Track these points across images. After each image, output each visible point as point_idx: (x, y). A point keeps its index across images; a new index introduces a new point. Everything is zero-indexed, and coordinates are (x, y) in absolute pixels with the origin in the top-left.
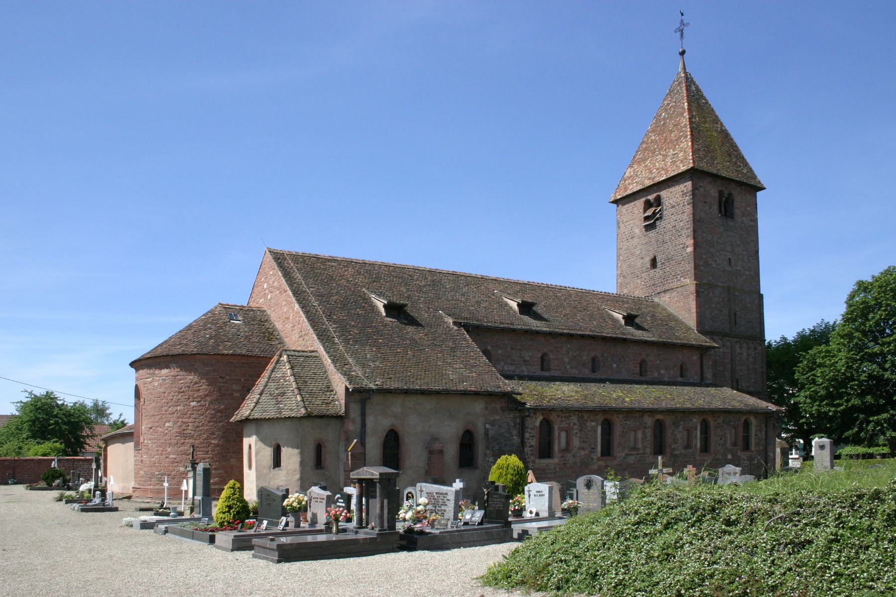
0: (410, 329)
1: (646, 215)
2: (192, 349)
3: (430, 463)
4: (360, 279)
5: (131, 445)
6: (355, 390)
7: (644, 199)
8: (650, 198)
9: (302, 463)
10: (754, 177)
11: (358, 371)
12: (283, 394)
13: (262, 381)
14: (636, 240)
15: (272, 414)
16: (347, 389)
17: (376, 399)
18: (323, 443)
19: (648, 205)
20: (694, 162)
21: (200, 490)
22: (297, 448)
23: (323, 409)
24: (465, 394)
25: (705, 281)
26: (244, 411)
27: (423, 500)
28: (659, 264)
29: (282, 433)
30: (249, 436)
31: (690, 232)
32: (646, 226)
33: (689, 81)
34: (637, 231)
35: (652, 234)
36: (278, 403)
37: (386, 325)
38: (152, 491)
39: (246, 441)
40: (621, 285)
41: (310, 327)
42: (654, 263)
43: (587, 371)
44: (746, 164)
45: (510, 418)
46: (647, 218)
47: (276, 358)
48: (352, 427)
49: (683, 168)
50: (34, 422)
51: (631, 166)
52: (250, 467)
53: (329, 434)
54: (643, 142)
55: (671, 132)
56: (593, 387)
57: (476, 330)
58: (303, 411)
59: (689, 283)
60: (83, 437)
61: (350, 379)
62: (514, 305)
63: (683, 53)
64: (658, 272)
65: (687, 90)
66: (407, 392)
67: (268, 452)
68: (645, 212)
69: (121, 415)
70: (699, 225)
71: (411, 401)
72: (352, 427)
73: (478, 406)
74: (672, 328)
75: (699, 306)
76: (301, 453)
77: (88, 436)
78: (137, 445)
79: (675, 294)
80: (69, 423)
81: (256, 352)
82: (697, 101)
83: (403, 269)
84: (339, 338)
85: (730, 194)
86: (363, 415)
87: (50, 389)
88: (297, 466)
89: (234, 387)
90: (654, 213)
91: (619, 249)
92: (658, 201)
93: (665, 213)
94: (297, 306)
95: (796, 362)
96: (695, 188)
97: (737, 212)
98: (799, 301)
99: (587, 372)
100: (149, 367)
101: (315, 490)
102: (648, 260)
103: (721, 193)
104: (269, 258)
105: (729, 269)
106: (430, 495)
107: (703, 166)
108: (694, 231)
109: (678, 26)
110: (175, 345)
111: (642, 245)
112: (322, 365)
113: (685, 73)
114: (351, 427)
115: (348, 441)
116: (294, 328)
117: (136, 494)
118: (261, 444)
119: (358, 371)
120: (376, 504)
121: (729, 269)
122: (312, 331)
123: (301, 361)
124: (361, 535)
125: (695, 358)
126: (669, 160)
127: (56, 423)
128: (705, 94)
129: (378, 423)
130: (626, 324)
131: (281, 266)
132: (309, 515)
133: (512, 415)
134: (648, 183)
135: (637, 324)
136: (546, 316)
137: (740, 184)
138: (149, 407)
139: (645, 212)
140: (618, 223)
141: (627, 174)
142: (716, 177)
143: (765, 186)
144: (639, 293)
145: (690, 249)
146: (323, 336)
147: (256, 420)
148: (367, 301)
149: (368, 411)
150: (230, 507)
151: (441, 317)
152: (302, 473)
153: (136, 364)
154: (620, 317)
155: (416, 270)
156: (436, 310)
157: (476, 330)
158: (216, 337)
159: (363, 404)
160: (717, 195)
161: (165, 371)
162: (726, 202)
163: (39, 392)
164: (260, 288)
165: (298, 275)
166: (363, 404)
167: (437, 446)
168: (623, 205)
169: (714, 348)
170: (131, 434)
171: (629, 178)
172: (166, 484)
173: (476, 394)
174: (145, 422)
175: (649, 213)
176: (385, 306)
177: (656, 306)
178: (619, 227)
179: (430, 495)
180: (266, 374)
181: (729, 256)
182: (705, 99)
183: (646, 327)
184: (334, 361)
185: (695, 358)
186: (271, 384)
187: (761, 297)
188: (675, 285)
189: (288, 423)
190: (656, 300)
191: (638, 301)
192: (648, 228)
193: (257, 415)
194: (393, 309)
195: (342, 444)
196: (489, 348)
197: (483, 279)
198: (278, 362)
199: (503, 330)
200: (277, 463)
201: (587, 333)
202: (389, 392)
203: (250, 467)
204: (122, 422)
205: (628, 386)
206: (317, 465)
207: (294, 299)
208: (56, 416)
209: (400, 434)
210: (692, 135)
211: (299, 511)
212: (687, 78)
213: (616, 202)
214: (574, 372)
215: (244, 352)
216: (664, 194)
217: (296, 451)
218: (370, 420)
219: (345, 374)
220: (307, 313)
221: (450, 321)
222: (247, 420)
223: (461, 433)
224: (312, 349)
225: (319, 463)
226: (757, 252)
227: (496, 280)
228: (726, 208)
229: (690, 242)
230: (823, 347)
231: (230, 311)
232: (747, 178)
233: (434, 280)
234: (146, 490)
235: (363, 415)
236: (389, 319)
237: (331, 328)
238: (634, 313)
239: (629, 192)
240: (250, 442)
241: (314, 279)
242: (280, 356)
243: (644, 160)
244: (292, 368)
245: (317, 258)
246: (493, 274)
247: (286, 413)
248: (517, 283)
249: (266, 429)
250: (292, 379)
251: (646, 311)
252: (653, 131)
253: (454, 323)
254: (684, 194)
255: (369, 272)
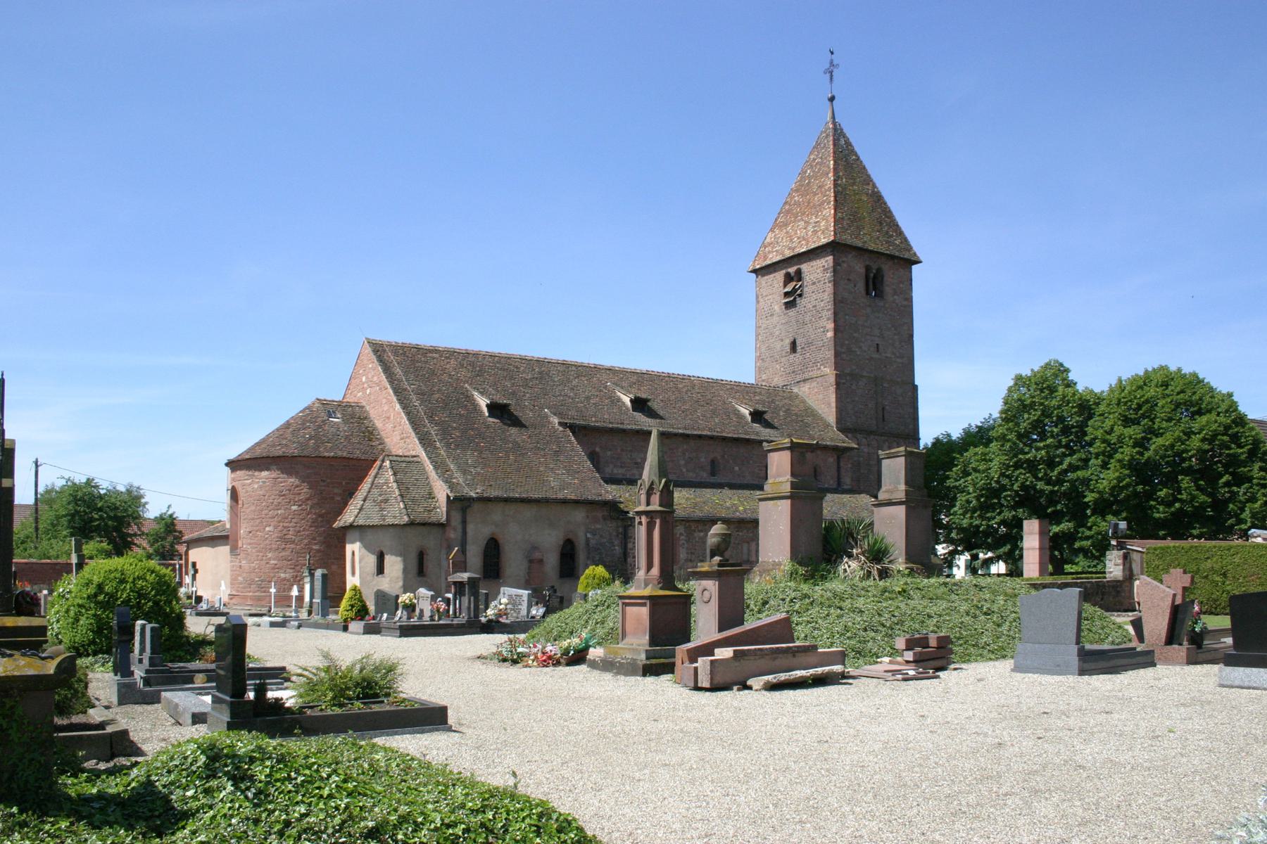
0: (513, 430)
1: (787, 290)
2: (293, 450)
3: (530, 572)
4: (463, 373)
5: (227, 549)
6: (456, 498)
7: (784, 271)
8: (789, 269)
9: (405, 571)
10: (909, 248)
11: (459, 478)
12: (386, 501)
13: (365, 486)
14: (775, 319)
15: (375, 521)
16: (448, 497)
17: (476, 507)
18: (423, 545)
19: (788, 279)
20: (835, 234)
21: (318, 593)
22: (400, 555)
23: (424, 517)
24: (565, 502)
25: (848, 371)
26: (348, 517)
27: (504, 600)
28: (799, 348)
29: (386, 540)
30: (353, 542)
31: (830, 314)
32: (786, 304)
33: (838, 133)
34: (776, 308)
35: (792, 312)
36: (382, 510)
37: (488, 427)
38: (252, 598)
39: (349, 548)
40: (759, 370)
41: (411, 431)
42: (793, 346)
43: (705, 475)
44: (900, 233)
45: (611, 527)
46: (787, 294)
47: (378, 463)
48: (453, 535)
49: (824, 241)
50: (73, 516)
51: (772, 230)
52: (353, 574)
53: (431, 541)
54: (786, 203)
55: (815, 194)
56: (708, 493)
57: (580, 431)
58: (406, 519)
59: (829, 372)
60: (131, 535)
61: (452, 487)
62: (627, 400)
63: (832, 99)
64: (796, 358)
65: (834, 145)
66: (507, 500)
67: (372, 560)
68: (785, 286)
69: (169, 507)
70: (840, 304)
71: (511, 509)
72: (453, 535)
73: (579, 515)
74: (807, 425)
75: (838, 399)
76: (404, 561)
77: (135, 535)
78: (234, 550)
79: (814, 384)
80: (115, 518)
81: (357, 454)
82: (846, 160)
83: (508, 358)
84: (441, 441)
85: (879, 270)
86: (464, 522)
87: (92, 475)
88: (400, 574)
89: (336, 491)
90: (794, 290)
91: (758, 327)
92: (799, 275)
93: (806, 289)
94: (398, 406)
95: (950, 464)
96: (836, 264)
97: (888, 290)
98: (956, 394)
99: (704, 476)
100: (249, 468)
101: (422, 591)
102: (787, 342)
103: (868, 269)
104: (368, 350)
105: (876, 356)
106: (510, 596)
107: (847, 238)
108: (835, 314)
109: (827, 66)
110: (274, 446)
111: (781, 324)
112: (423, 471)
113: (834, 123)
114: (452, 535)
115: (450, 549)
116: (395, 430)
117: (234, 601)
118: (364, 550)
119: (459, 478)
120: (465, 600)
121: (876, 356)
122: (413, 434)
123: (403, 466)
124: (456, 621)
125: (831, 460)
126: (810, 228)
127: (101, 518)
128: (856, 149)
129: (478, 532)
130: (753, 421)
131: (381, 360)
132: (417, 611)
133: (614, 524)
134: (788, 254)
135: (766, 421)
136: (661, 413)
137: (892, 257)
138: (247, 509)
139: (785, 286)
140: (757, 297)
141: (768, 240)
142: (861, 251)
143: (922, 258)
144: (778, 381)
145: (830, 334)
146: (425, 440)
147: (360, 527)
148: (470, 399)
149: (469, 519)
150: (352, 606)
151: (547, 417)
152: (405, 581)
153: (233, 465)
154: (746, 412)
155: (523, 359)
156: (542, 408)
157: (580, 431)
158: (315, 437)
159: (464, 511)
160: (863, 271)
161: (265, 473)
162: (875, 277)
163: (80, 479)
164: (358, 381)
165: (398, 371)
166: (464, 511)
167: (537, 555)
168: (763, 275)
169: (853, 449)
170: (227, 537)
171: (770, 244)
172: (273, 590)
173: (576, 502)
174: (243, 526)
175: (788, 289)
176: (487, 406)
177: (793, 397)
178: (758, 302)
179: (510, 596)
180: (369, 479)
181: (877, 340)
182: (856, 154)
183: (776, 425)
184: (436, 468)
185: (831, 460)
186: (375, 491)
187: (915, 388)
188: (815, 373)
189: (391, 530)
190: (795, 390)
191: (773, 392)
192: (789, 305)
193: (361, 522)
194: (495, 409)
195: (444, 552)
196: (597, 449)
197: (597, 369)
198: (381, 467)
199: (612, 431)
200: (380, 570)
201: (704, 433)
202: (488, 500)
203: (353, 574)
204: (171, 516)
205: (747, 492)
206: (419, 571)
207: (395, 399)
208: (100, 509)
209: (501, 542)
210: (836, 200)
211: (410, 608)
212: (835, 129)
213: (755, 271)
214: (691, 476)
215: (345, 454)
216: (805, 267)
217: (399, 559)
218: (471, 528)
219: (446, 482)
220: (408, 414)
221: (555, 420)
222: (351, 526)
223: (561, 543)
224: (414, 453)
225: (421, 571)
226: (912, 336)
227: (610, 369)
228: (874, 283)
229: (831, 325)
230: (980, 450)
231: (329, 407)
232: (900, 251)
233: (542, 370)
234: (245, 598)
235: (464, 522)
236: (491, 420)
237: (434, 431)
238: (760, 408)
239: (768, 262)
240: (353, 549)
241: (416, 371)
242: (383, 461)
243: (786, 225)
244: (395, 474)
245: (418, 348)
246: (607, 362)
247: (390, 521)
248: (634, 373)
249: (370, 535)
250: (395, 485)
251: (781, 404)
252: (797, 191)
253: (560, 424)
254: (825, 270)
255: (472, 364)
